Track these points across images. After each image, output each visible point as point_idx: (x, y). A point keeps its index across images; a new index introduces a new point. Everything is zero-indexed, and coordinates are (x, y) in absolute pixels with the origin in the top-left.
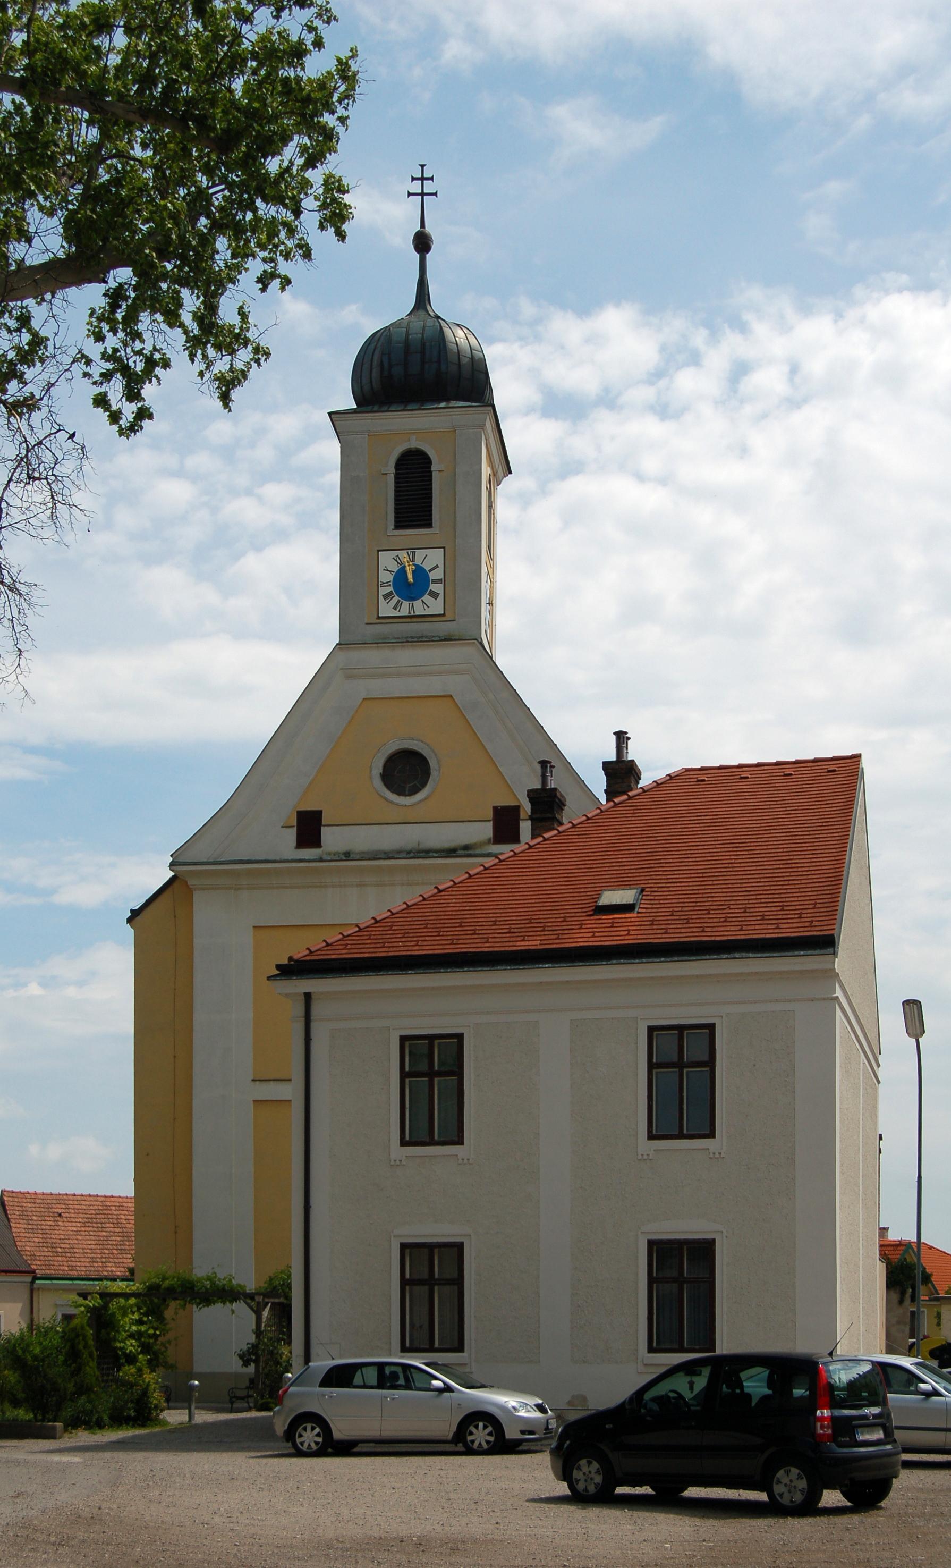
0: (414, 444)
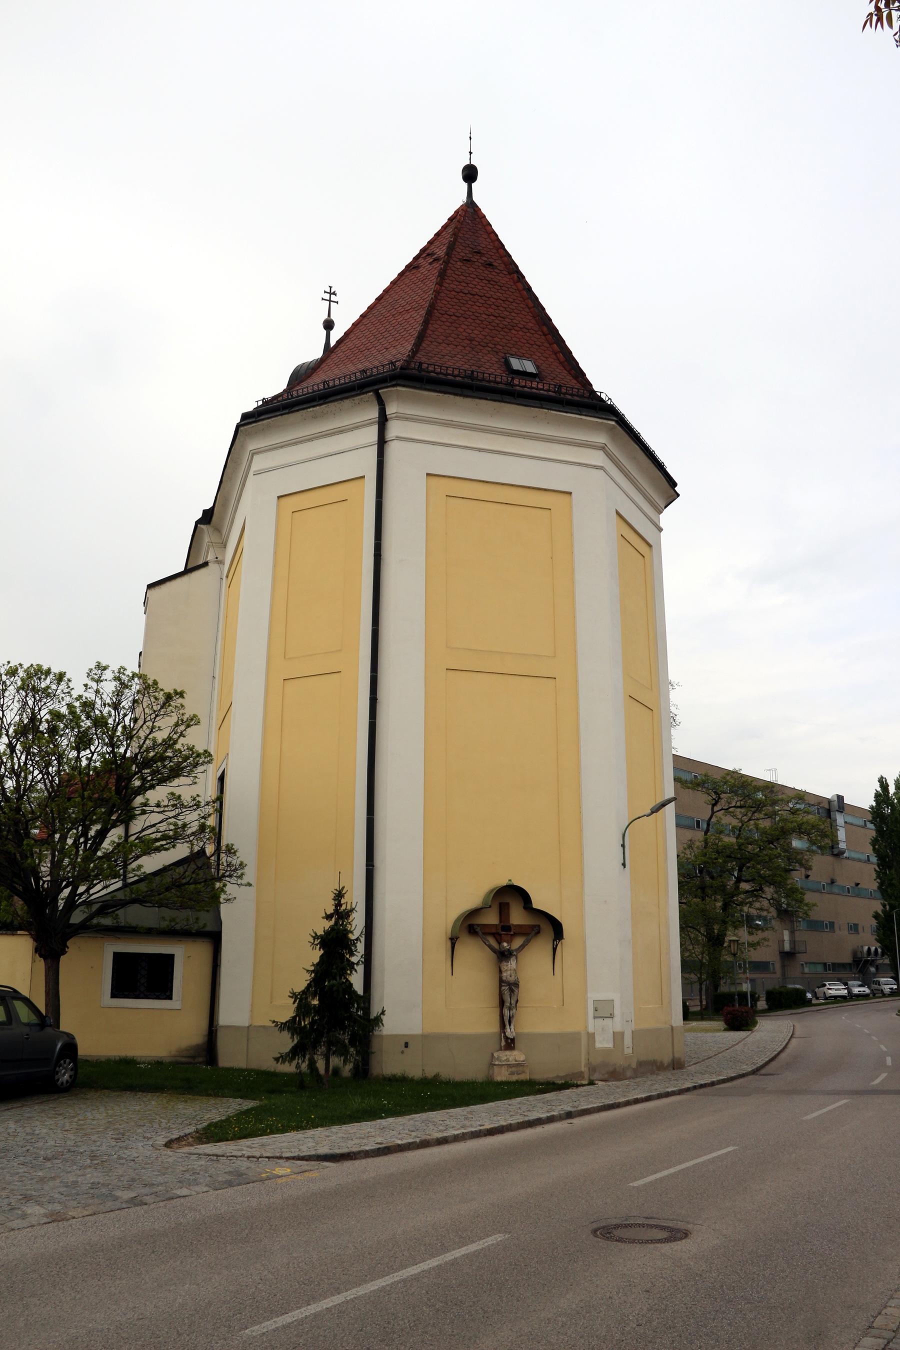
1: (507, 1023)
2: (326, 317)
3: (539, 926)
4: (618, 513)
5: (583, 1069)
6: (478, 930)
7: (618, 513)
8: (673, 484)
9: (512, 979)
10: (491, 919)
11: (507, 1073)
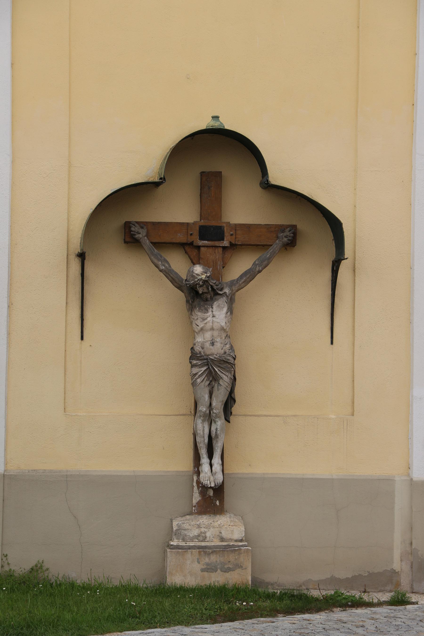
1: (203, 452)
3: (294, 227)
5: (396, 566)
6: (141, 235)
9: (217, 350)
10: (180, 209)
11: (197, 567)
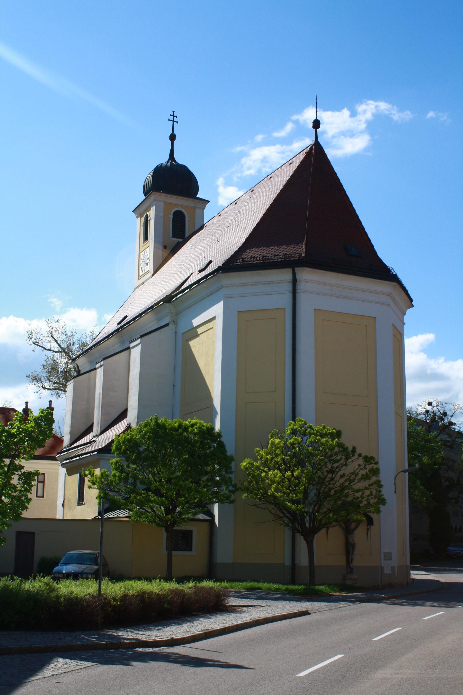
0: (180, 209)
2: (171, 132)
4: (393, 325)
7: (393, 325)
8: (411, 300)
